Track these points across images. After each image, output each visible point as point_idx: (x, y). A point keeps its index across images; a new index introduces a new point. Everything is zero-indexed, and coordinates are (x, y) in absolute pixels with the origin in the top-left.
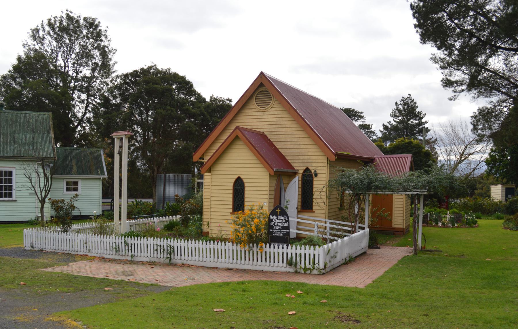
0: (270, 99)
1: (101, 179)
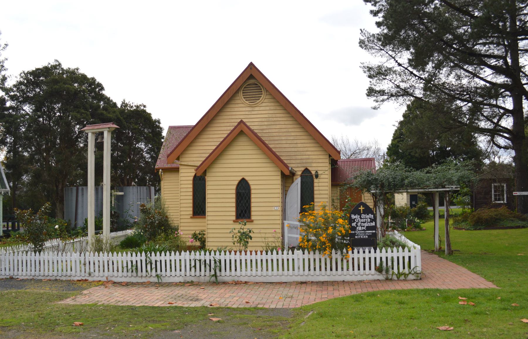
0: (260, 93)
1: (3, 193)
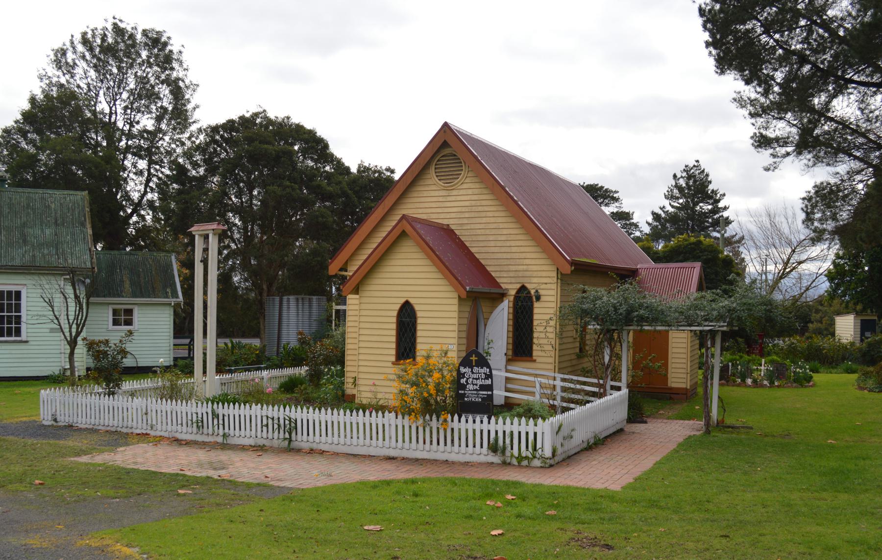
0: (459, 169)
1: (173, 304)
